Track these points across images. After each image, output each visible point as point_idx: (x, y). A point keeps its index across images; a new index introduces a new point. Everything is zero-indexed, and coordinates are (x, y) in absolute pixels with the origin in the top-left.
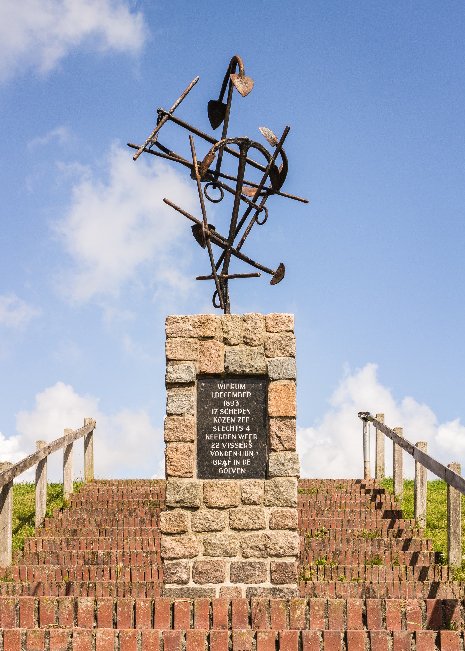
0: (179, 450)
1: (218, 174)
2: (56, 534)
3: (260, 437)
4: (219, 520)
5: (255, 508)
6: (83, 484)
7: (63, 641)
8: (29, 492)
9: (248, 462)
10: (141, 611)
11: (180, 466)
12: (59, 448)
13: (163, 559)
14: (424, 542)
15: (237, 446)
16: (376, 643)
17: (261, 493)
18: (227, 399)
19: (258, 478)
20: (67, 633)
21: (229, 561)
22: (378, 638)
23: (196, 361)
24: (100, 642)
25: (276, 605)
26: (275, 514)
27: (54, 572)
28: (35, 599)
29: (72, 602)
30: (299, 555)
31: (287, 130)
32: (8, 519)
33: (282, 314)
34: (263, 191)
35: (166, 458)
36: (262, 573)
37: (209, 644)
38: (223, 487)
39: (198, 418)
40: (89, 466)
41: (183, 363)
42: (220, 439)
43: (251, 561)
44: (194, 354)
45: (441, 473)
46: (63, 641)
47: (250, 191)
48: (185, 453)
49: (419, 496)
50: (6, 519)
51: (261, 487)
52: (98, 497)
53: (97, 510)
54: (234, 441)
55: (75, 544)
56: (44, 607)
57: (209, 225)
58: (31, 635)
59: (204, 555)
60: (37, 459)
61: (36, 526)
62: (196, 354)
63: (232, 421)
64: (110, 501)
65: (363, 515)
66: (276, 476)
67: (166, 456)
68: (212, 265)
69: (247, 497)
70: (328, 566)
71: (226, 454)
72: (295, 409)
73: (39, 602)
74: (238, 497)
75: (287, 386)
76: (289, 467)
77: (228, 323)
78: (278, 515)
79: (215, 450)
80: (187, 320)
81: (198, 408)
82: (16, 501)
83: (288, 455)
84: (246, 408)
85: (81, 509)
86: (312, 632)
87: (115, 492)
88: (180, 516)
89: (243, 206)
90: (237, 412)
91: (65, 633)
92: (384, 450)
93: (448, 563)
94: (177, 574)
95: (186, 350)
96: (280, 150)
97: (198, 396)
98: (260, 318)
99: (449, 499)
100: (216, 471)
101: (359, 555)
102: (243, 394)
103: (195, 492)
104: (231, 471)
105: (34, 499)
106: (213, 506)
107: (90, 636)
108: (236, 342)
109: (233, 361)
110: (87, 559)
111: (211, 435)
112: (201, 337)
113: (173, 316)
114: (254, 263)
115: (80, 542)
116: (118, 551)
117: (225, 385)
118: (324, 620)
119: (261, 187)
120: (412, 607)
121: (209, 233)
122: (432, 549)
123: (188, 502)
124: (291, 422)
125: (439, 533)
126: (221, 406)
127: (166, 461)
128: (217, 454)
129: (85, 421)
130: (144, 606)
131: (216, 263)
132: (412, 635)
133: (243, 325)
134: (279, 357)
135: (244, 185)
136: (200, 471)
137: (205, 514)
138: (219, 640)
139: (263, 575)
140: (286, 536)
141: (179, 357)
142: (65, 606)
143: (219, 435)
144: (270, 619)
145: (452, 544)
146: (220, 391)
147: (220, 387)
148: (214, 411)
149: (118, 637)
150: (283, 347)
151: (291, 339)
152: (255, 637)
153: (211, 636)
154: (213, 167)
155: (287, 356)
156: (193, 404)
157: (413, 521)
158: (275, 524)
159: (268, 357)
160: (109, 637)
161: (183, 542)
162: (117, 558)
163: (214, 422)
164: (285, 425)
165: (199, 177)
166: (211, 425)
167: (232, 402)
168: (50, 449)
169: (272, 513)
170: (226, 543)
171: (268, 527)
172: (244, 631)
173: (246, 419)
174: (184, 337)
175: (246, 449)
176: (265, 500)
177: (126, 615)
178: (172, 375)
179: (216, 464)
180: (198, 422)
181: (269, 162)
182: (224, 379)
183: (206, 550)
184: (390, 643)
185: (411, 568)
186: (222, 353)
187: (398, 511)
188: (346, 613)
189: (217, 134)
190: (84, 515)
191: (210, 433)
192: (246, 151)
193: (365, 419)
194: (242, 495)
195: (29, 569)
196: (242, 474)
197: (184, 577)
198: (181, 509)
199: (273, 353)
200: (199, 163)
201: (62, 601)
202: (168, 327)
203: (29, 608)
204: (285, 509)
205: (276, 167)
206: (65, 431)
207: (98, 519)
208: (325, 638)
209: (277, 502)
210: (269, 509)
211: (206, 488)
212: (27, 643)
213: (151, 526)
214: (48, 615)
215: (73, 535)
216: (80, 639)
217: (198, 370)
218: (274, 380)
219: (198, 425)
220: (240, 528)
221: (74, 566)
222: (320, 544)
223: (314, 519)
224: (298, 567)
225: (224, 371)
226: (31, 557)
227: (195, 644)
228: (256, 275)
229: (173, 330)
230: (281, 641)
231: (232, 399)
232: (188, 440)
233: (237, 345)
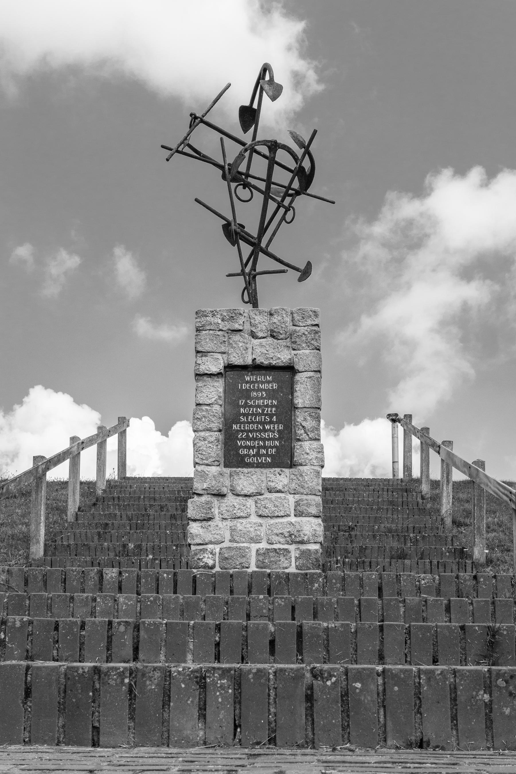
1: (248, 175)
4: (245, 507)
7: (86, 605)
9: (274, 451)
10: (164, 583)
11: (208, 455)
17: (286, 481)
18: (254, 390)
19: (283, 468)
21: (254, 547)
23: (224, 353)
25: (294, 578)
27: (85, 564)
29: (97, 573)
30: (323, 542)
32: (41, 511)
36: (286, 559)
41: (211, 355)
45: (466, 470)
50: (39, 512)
53: (129, 505)
55: (106, 537)
58: (56, 599)
62: (225, 346)
64: (142, 497)
65: (390, 512)
66: (301, 465)
67: (194, 445)
71: (253, 444)
73: (66, 573)
74: (264, 485)
77: (256, 317)
79: (242, 439)
80: (216, 313)
82: (50, 497)
84: (273, 399)
85: (113, 504)
88: (207, 503)
89: (272, 206)
94: (203, 560)
95: (215, 342)
98: (287, 312)
100: (243, 460)
102: (270, 386)
104: (257, 459)
108: (264, 335)
113: (203, 309)
115: (111, 535)
116: (148, 544)
118: (341, 593)
119: (289, 188)
120: (426, 581)
125: (464, 530)
126: (249, 397)
128: (244, 444)
130: (167, 577)
131: (244, 261)
133: (270, 319)
136: (227, 460)
137: (231, 502)
138: (237, 606)
139: (287, 561)
141: (207, 349)
142: (91, 577)
144: (289, 591)
146: (247, 382)
147: (247, 378)
148: (242, 402)
155: (313, 349)
158: (300, 511)
159: (294, 350)
160: (131, 602)
161: (210, 529)
162: (147, 551)
167: (259, 394)
170: (252, 529)
171: (292, 515)
172: (261, 597)
173: (272, 410)
174: (213, 330)
175: (273, 439)
177: (150, 586)
181: (297, 164)
188: (362, 586)
190: (116, 510)
191: (236, 423)
192: (275, 153)
193: (394, 421)
195: (60, 560)
197: (210, 562)
200: (229, 165)
202: (198, 320)
203: (56, 578)
205: (303, 169)
209: (302, 490)
212: (53, 607)
213: (182, 521)
216: (103, 603)
217: (226, 362)
220: (266, 515)
221: (105, 558)
222: (347, 539)
223: (342, 516)
225: (252, 363)
226: (63, 549)
227: (214, 610)
229: (203, 323)
231: (259, 390)
233: (264, 338)
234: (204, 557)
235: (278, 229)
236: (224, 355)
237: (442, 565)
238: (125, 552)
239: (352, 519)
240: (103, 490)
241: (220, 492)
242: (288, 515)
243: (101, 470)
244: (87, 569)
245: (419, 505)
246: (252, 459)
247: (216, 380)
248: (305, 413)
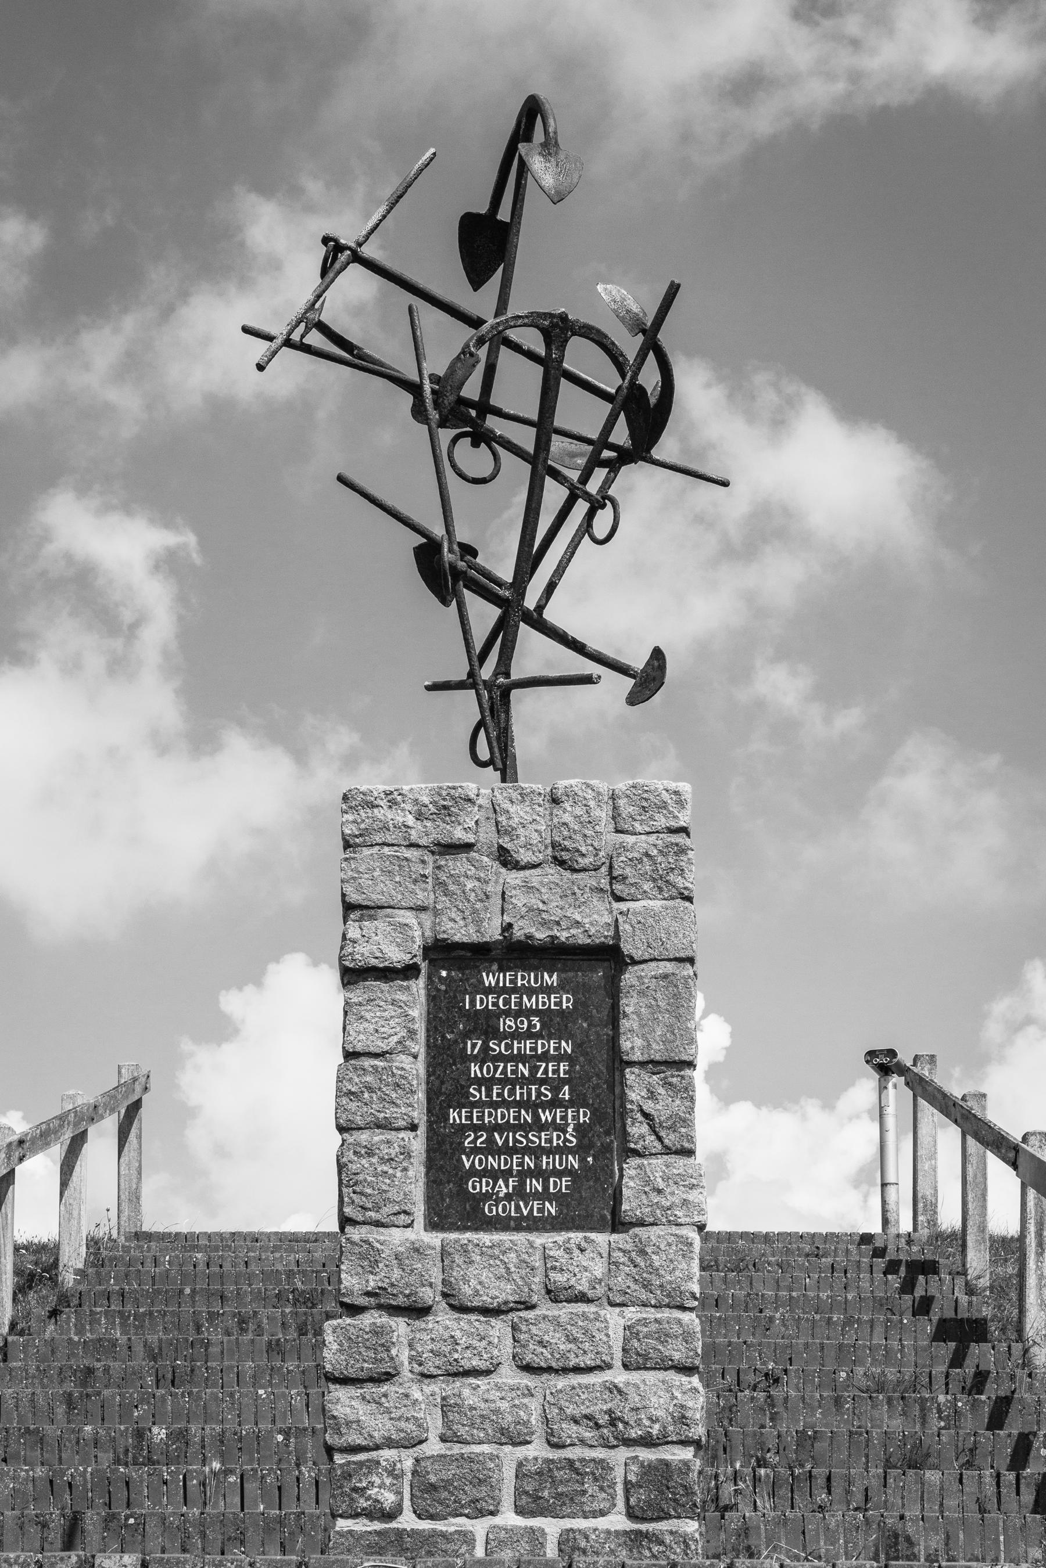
0: (377, 1151)
1: (485, 407)
2: (36, 1381)
3: (598, 1116)
4: (484, 1343)
5: (584, 1312)
9: (564, 1183)
12: (47, 1145)
13: (330, 1450)
15: (533, 1142)
17: (599, 1269)
18: (507, 1013)
19: (592, 1229)
21: (510, 1455)
23: (423, 909)
26: (639, 1328)
27: (30, 1485)
34: (607, 454)
35: (340, 1173)
36: (602, 1489)
38: (497, 1252)
41: (387, 916)
42: (490, 1122)
43: (570, 1456)
44: (418, 891)
47: (573, 455)
48: (392, 1159)
51: (600, 1254)
52: (153, 1278)
53: (151, 1313)
54: (525, 1128)
55: (90, 1407)
57: (460, 545)
62: (425, 890)
63: (522, 1073)
64: (188, 1291)
65: (879, 1330)
67: (341, 1167)
68: (468, 652)
69: (561, 1279)
71: (506, 1164)
74: (537, 1280)
75: (672, 978)
78: (645, 1330)
79: (476, 1151)
80: (399, 798)
81: (428, 1037)
83: (674, 1167)
84: (560, 1039)
85: (106, 1313)
87: (201, 1267)
88: (377, 1331)
89: (554, 494)
95: (397, 879)
96: (652, 346)
97: (428, 1005)
98: (599, 793)
100: (477, 1210)
101: (868, 1440)
103: (420, 1265)
104: (518, 1207)
106: (469, 1304)
109: (524, 909)
111: (464, 1110)
112: (439, 844)
113: (363, 788)
116: (207, 1427)
117: (501, 975)
119: (603, 442)
121: (462, 565)
123: (401, 1293)
124: (683, 1077)
128: (480, 1164)
131: (478, 646)
133: (551, 814)
134: (649, 902)
136: (433, 1209)
137: (447, 1328)
139: (604, 1495)
143: (486, 1111)
147: (489, 980)
148: (474, 1046)
150: (661, 872)
151: (682, 851)
154: (471, 390)
155: (672, 898)
156: (416, 1026)
158: (638, 1354)
159: (619, 899)
161: (386, 1405)
162: (203, 1447)
163: (473, 1076)
164: (665, 1083)
165: (434, 415)
166: (463, 1083)
167: (522, 1022)
169: (629, 1323)
170: (504, 1405)
171: (618, 1363)
173: (559, 1069)
174: (393, 845)
175: (562, 1150)
176: (610, 1289)
178: (358, 948)
179: (478, 1190)
180: (429, 1075)
183: (447, 1423)
185: (1011, 1476)
187: (976, 1321)
190: (115, 1330)
192: (562, 348)
193: (884, 1070)
194: (547, 1276)
196: (547, 1218)
197: (388, 1499)
198: (380, 1312)
200: (435, 379)
202: (350, 817)
204: (666, 1315)
205: (642, 390)
209: (644, 1295)
211: (450, 1254)
213: (299, 1358)
215: (84, 1384)
217: (428, 933)
218: (635, 962)
219: (428, 1083)
220: (543, 1364)
221: (85, 1470)
222: (762, 1409)
223: (745, 1343)
224: (700, 1473)
225: (501, 938)
228: (587, 680)
229: (363, 826)
231: (522, 1012)
232: (401, 1123)
233: (534, 866)
234: (372, 1484)
235: (571, 556)
236: (423, 916)
237: (1028, 1485)
238: (142, 1449)
239: (775, 1351)
240: (78, 1272)
241: (415, 1301)
242: (609, 1366)
243: (71, 1214)
244: (49, 1558)
245: (959, 1311)
246: (504, 1206)
247: (401, 986)
248: (650, 1077)
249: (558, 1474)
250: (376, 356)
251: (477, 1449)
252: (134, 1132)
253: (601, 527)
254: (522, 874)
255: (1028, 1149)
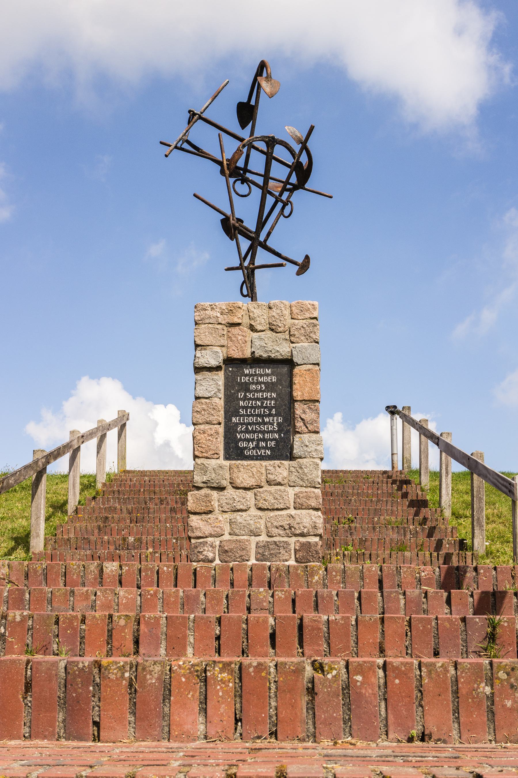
1: (246, 170)
2: (88, 521)
3: (285, 420)
4: (244, 500)
6: (116, 475)
8: (62, 482)
12: (92, 438)
13: (190, 538)
14: (449, 530)
16: (388, 602)
17: (285, 473)
18: (253, 383)
19: (283, 460)
20: (91, 591)
21: (254, 540)
22: (390, 597)
23: (223, 346)
24: (123, 600)
27: (85, 557)
28: (62, 564)
31: (312, 128)
32: (41, 505)
33: (307, 302)
34: (288, 186)
35: (193, 440)
36: (286, 552)
37: (228, 602)
38: (249, 467)
39: (225, 402)
40: (122, 457)
43: (275, 540)
46: (87, 599)
47: (277, 187)
49: (444, 486)
52: (130, 486)
53: (129, 498)
54: (259, 424)
55: (106, 530)
56: (71, 572)
57: (237, 218)
59: (230, 534)
60: (71, 447)
61: (69, 514)
64: (142, 490)
65: (389, 504)
68: (239, 255)
70: (354, 552)
71: (252, 436)
72: (318, 393)
74: (263, 477)
76: (313, 449)
77: (255, 311)
78: (302, 495)
79: (241, 432)
80: (215, 307)
82: (50, 490)
84: (272, 392)
85: (113, 498)
86: (327, 592)
87: (147, 482)
88: (207, 496)
89: (270, 200)
90: (262, 396)
91: (89, 591)
92: (410, 442)
93: (473, 550)
96: (304, 147)
98: (285, 305)
99: (472, 487)
101: (385, 542)
104: (257, 452)
105: (68, 489)
107: (113, 595)
108: (262, 329)
109: (259, 346)
110: (118, 545)
112: (229, 323)
113: (202, 304)
114: (281, 254)
116: (148, 537)
119: (287, 182)
120: (426, 573)
121: (237, 225)
122: (458, 537)
124: (315, 406)
126: (248, 390)
127: (194, 442)
129: (118, 413)
132: (423, 595)
135: (270, 180)
137: (231, 495)
139: (287, 554)
140: (310, 516)
141: (207, 342)
145: (476, 531)
146: (246, 375)
147: (247, 371)
148: (241, 395)
149: (140, 595)
151: (315, 325)
152: (273, 596)
153: (230, 594)
154: (241, 163)
156: (221, 388)
157: (439, 510)
158: (299, 504)
159: (292, 343)
162: (147, 544)
165: (227, 172)
168: (84, 438)
170: (252, 522)
171: (292, 507)
175: (272, 432)
178: (200, 360)
180: (225, 405)
181: (294, 159)
182: (250, 364)
183: (232, 529)
184: (402, 602)
185: (435, 554)
186: (248, 339)
187: (424, 500)
189: (245, 134)
192: (273, 148)
193: (393, 413)
197: (210, 555)
199: (297, 339)
201: (88, 565)
202: (197, 314)
203: (56, 572)
206: (99, 421)
207: (129, 507)
208: (339, 597)
209: (301, 483)
210: (293, 490)
214: (74, 579)
215: (105, 522)
217: (225, 355)
218: (298, 365)
219: (225, 408)
220: (266, 508)
222: (347, 531)
224: (321, 546)
228: (281, 265)
229: (202, 317)
230: (297, 600)
231: (258, 383)
232: (215, 422)
233: (263, 331)
236: (223, 349)
242: (289, 508)
249: (271, 547)
250: (207, 152)
251: (242, 537)
252: (123, 434)
253: (287, 212)
254: (258, 334)
255: (443, 438)
